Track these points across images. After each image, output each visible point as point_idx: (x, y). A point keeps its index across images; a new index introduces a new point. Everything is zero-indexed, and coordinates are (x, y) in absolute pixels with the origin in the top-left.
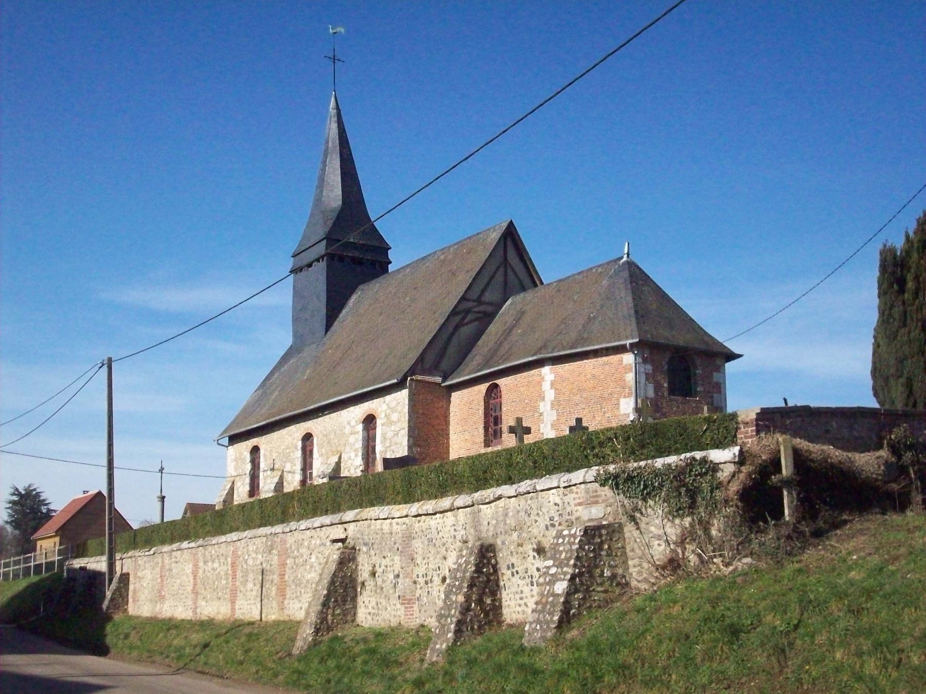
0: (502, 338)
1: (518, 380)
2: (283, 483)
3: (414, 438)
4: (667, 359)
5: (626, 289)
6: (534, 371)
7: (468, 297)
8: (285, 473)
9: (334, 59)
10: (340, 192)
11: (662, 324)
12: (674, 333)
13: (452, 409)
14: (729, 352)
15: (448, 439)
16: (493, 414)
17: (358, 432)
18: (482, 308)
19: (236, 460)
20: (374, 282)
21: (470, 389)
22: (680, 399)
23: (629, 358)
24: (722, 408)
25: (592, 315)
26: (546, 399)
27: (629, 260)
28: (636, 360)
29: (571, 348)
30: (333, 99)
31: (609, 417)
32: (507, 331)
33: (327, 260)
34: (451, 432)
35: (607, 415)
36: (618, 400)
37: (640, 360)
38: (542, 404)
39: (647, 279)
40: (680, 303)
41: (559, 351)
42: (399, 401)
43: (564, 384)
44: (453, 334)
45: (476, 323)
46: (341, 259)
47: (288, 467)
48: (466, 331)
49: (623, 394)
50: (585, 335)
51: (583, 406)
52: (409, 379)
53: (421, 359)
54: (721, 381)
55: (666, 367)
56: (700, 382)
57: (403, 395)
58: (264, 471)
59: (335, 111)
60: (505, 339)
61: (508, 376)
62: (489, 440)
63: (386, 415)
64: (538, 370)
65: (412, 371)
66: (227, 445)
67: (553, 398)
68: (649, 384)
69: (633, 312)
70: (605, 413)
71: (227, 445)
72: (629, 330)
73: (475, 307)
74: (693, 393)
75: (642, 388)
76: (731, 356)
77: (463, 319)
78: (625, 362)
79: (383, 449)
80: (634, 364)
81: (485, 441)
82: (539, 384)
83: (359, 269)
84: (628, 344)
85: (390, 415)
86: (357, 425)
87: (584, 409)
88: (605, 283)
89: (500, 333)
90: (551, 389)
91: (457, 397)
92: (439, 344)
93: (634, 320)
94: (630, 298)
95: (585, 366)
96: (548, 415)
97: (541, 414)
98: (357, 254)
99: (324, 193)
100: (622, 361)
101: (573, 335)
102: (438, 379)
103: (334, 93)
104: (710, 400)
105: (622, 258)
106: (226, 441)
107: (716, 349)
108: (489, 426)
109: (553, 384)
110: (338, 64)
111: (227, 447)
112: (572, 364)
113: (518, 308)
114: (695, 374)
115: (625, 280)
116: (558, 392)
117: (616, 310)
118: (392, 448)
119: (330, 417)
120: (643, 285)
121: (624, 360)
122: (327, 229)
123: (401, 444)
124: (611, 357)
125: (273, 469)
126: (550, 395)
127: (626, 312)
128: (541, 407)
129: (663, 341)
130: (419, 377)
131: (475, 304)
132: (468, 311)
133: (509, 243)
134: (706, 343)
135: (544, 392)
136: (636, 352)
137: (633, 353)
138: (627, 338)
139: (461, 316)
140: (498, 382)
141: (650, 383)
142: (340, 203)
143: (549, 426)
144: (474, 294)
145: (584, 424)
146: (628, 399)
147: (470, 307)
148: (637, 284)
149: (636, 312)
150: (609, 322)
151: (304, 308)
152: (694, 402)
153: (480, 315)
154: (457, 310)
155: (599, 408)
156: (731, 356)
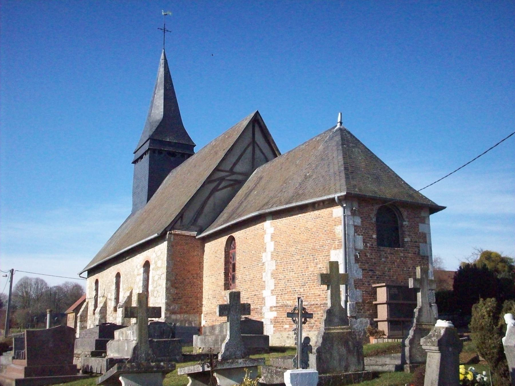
0: (243, 199)
1: (248, 233)
2: (106, 307)
3: (171, 281)
4: (375, 212)
5: (338, 150)
6: (258, 225)
7: (221, 168)
8: (108, 300)
9: (164, 30)
10: (162, 110)
11: (370, 179)
12: (381, 187)
13: (205, 257)
14: (433, 204)
15: (202, 281)
16: (232, 262)
17: (141, 274)
18: (234, 177)
19: (89, 288)
20: (178, 167)
21: (216, 241)
22: (388, 250)
23: (338, 211)
24: (428, 257)
25: (308, 174)
26: (267, 250)
27: (341, 127)
28: (344, 213)
29: (287, 204)
30: (163, 54)
31: (320, 268)
32: (248, 193)
33: (150, 153)
34: (204, 276)
35: (319, 266)
36: (329, 251)
37: (349, 213)
38: (264, 255)
39: (357, 142)
40: (386, 163)
41: (277, 206)
42: (162, 251)
43: (282, 237)
44: (208, 198)
45: (229, 188)
46: (160, 152)
47: (109, 297)
48: (220, 195)
49: (333, 246)
50: (300, 192)
51: (298, 257)
52: (168, 233)
53: (181, 216)
54: (426, 231)
55: (374, 220)
56: (407, 233)
57: (163, 248)
58: (99, 297)
59: (163, 61)
60: (245, 199)
61: (240, 229)
62: (228, 284)
63: (155, 261)
64: (262, 224)
65: (172, 226)
66: (87, 277)
67: (272, 250)
68: (357, 236)
69: (343, 169)
70: (317, 264)
71: (87, 277)
72: (338, 185)
73: (227, 176)
74: (401, 244)
75: (351, 240)
76: (435, 209)
77: (219, 184)
78: (334, 215)
79: (153, 289)
80: (342, 217)
81: (225, 284)
82: (262, 236)
83: (172, 159)
84: (336, 198)
85: (157, 262)
86: (140, 268)
87: (299, 260)
88: (321, 147)
89: (243, 196)
90: (272, 241)
91: (209, 246)
92: (197, 205)
93: (343, 175)
94: (341, 157)
95: (299, 220)
96: (268, 265)
97: (263, 264)
98: (171, 149)
99: (153, 111)
100: (332, 214)
101: (291, 192)
102: (195, 233)
103: (163, 50)
104: (417, 250)
105: (336, 126)
106: (85, 274)
107: (421, 201)
108: (229, 271)
109: (272, 237)
110: (166, 33)
111: (86, 278)
112: (289, 218)
113: (259, 175)
114: (402, 226)
115: (337, 143)
116: (277, 244)
117: (328, 168)
118: (157, 288)
119: (128, 261)
120: (353, 147)
121: (334, 213)
122: (151, 133)
123: (162, 286)
124: (322, 211)
125: (104, 296)
126: (270, 246)
127: (336, 168)
128: (264, 258)
129: (371, 195)
130: (178, 232)
131: (227, 174)
132: (222, 179)
133: (257, 129)
134: (411, 196)
135: (265, 244)
136: (344, 205)
137: (342, 206)
138: (336, 192)
139: (215, 184)
140: (233, 235)
141: (359, 235)
142: (162, 117)
143: (269, 275)
144: (227, 166)
145: (243, 301)
146: (338, 251)
147: (223, 177)
148: (348, 146)
149: (346, 169)
150: (322, 179)
151: (138, 187)
152: (401, 252)
153: (232, 182)
154: (213, 178)
155: (312, 259)
156: (435, 209)
